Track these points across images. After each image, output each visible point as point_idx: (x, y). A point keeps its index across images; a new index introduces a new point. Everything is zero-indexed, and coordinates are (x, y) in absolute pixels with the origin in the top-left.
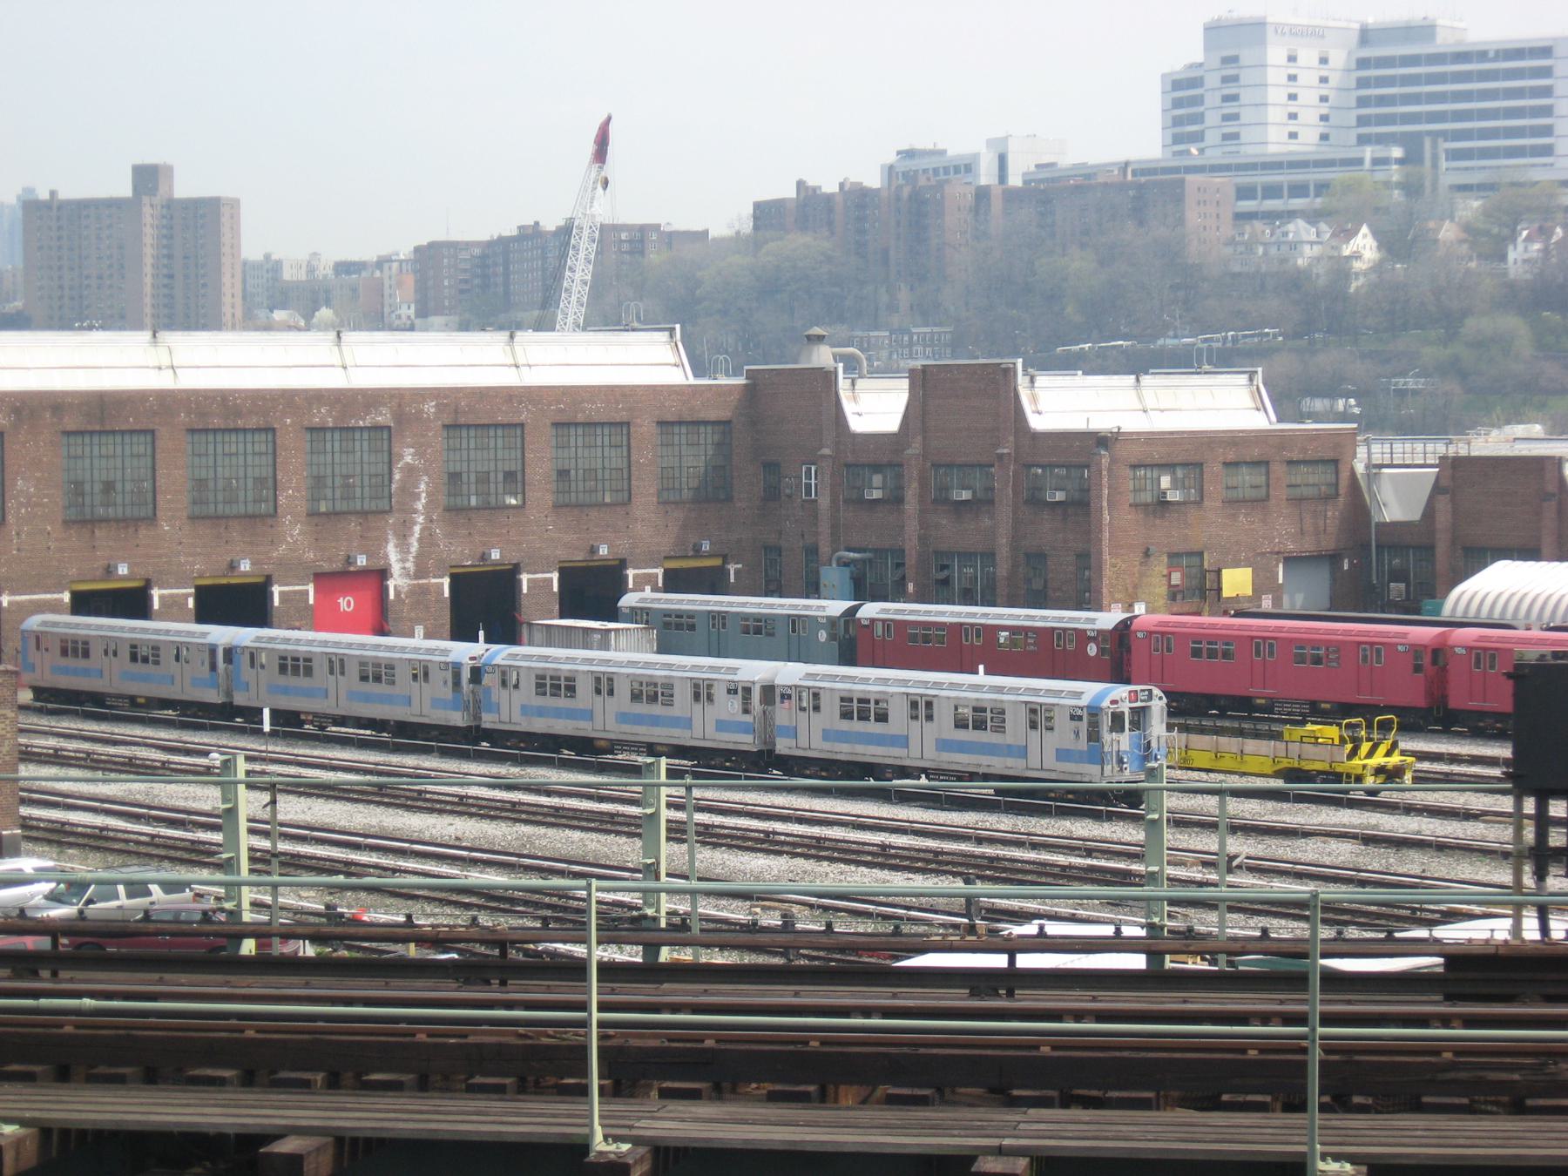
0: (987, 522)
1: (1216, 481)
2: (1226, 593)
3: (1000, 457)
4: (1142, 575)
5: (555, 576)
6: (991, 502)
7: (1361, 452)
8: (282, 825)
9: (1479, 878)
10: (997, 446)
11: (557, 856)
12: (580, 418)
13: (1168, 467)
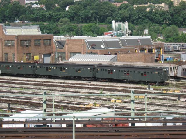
1: (32, 43)
2: (35, 59)
7: (54, 38)
13: (26, 40)
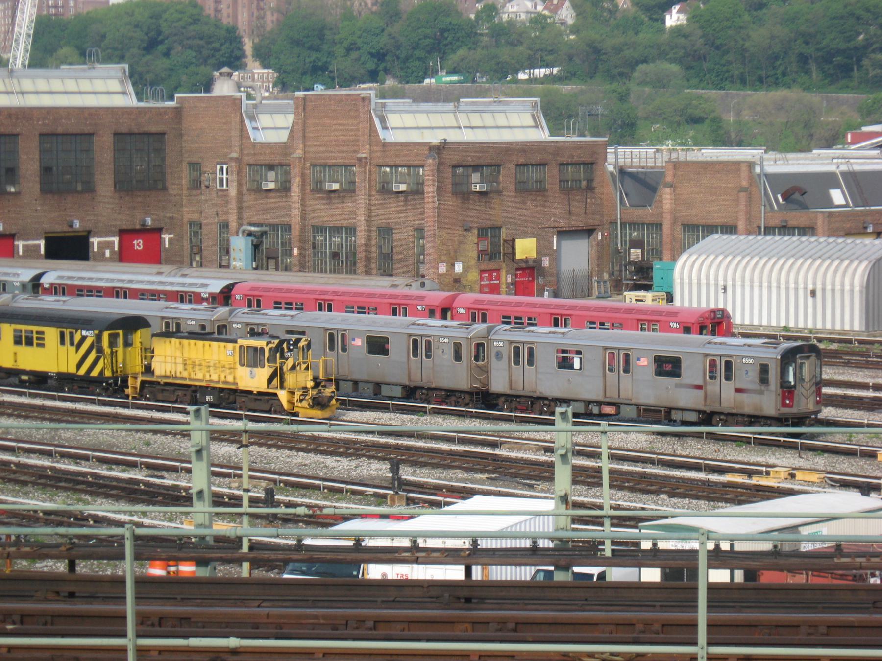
0: (349, 205)
1: (507, 178)
3: (360, 159)
4: (460, 243)
5: (42, 243)
6: (354, 191)
7: (611, 158)
8: (552, 499)
9: (740, 458)
10: (358, 152)
11: (79, 445)
12: (60, 130)
13: (476, 168)
